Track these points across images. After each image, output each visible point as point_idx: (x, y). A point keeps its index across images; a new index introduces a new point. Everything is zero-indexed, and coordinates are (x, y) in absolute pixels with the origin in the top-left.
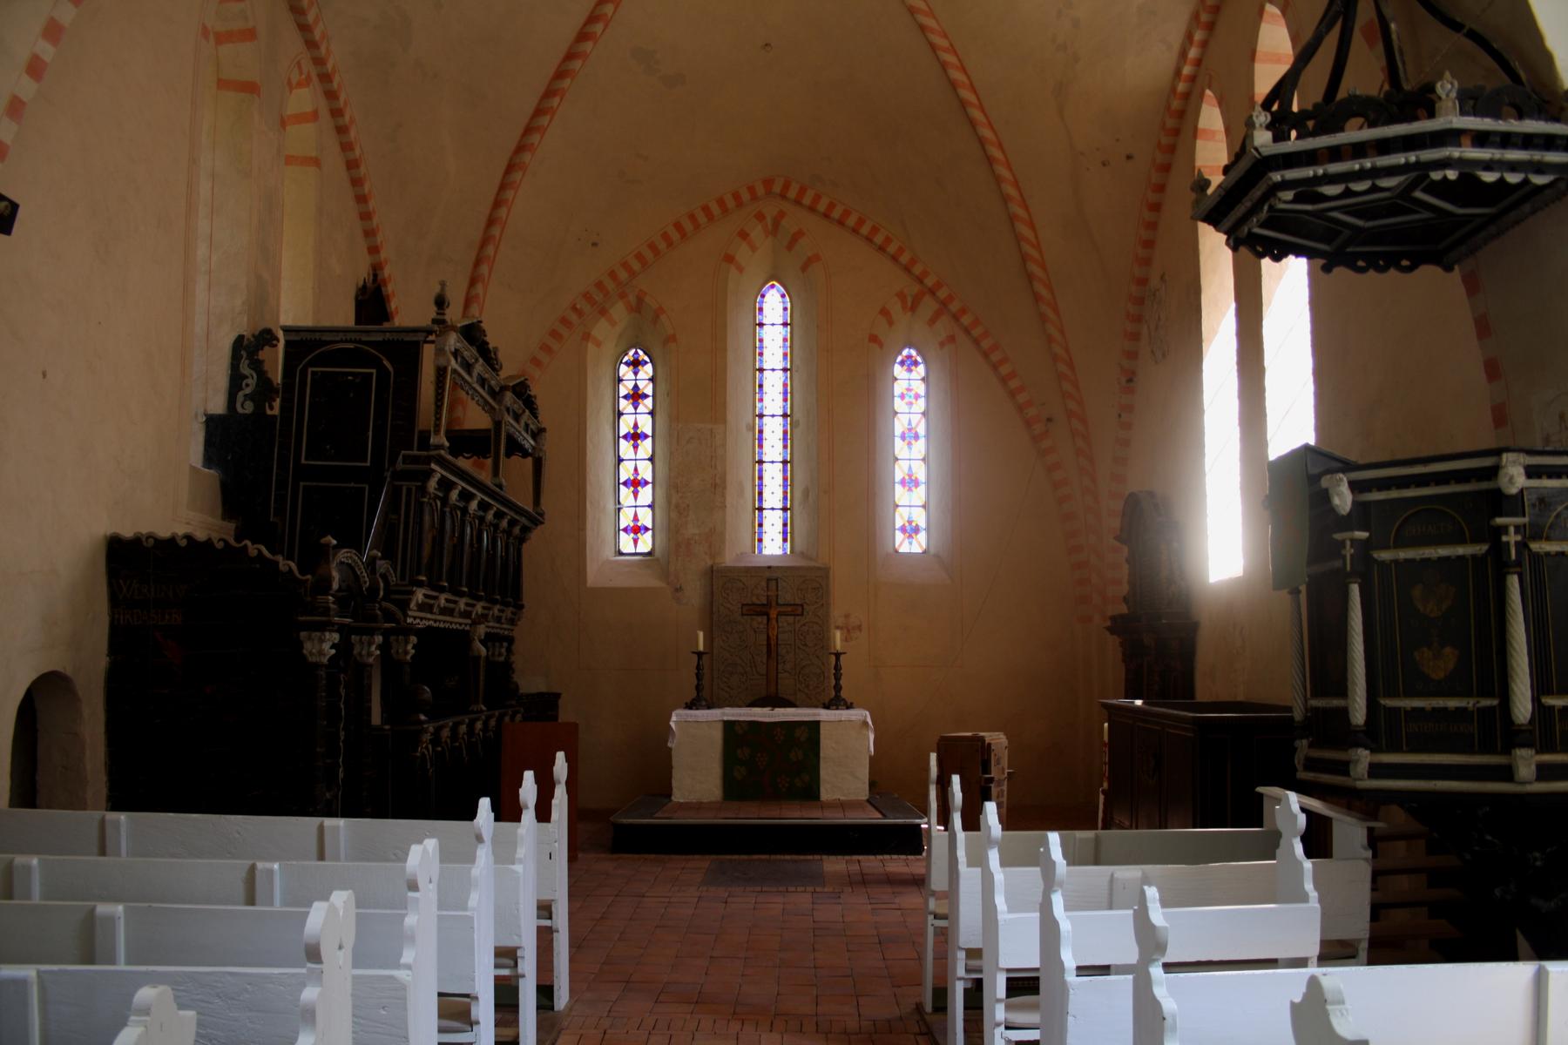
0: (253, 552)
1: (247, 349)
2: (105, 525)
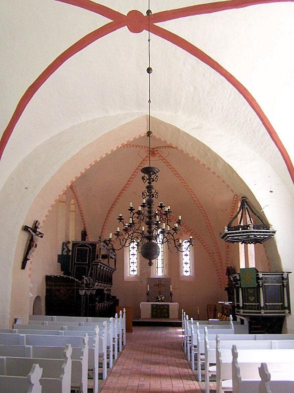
0: (71, 278)
1: (65, 244)
2: (46, 274)
